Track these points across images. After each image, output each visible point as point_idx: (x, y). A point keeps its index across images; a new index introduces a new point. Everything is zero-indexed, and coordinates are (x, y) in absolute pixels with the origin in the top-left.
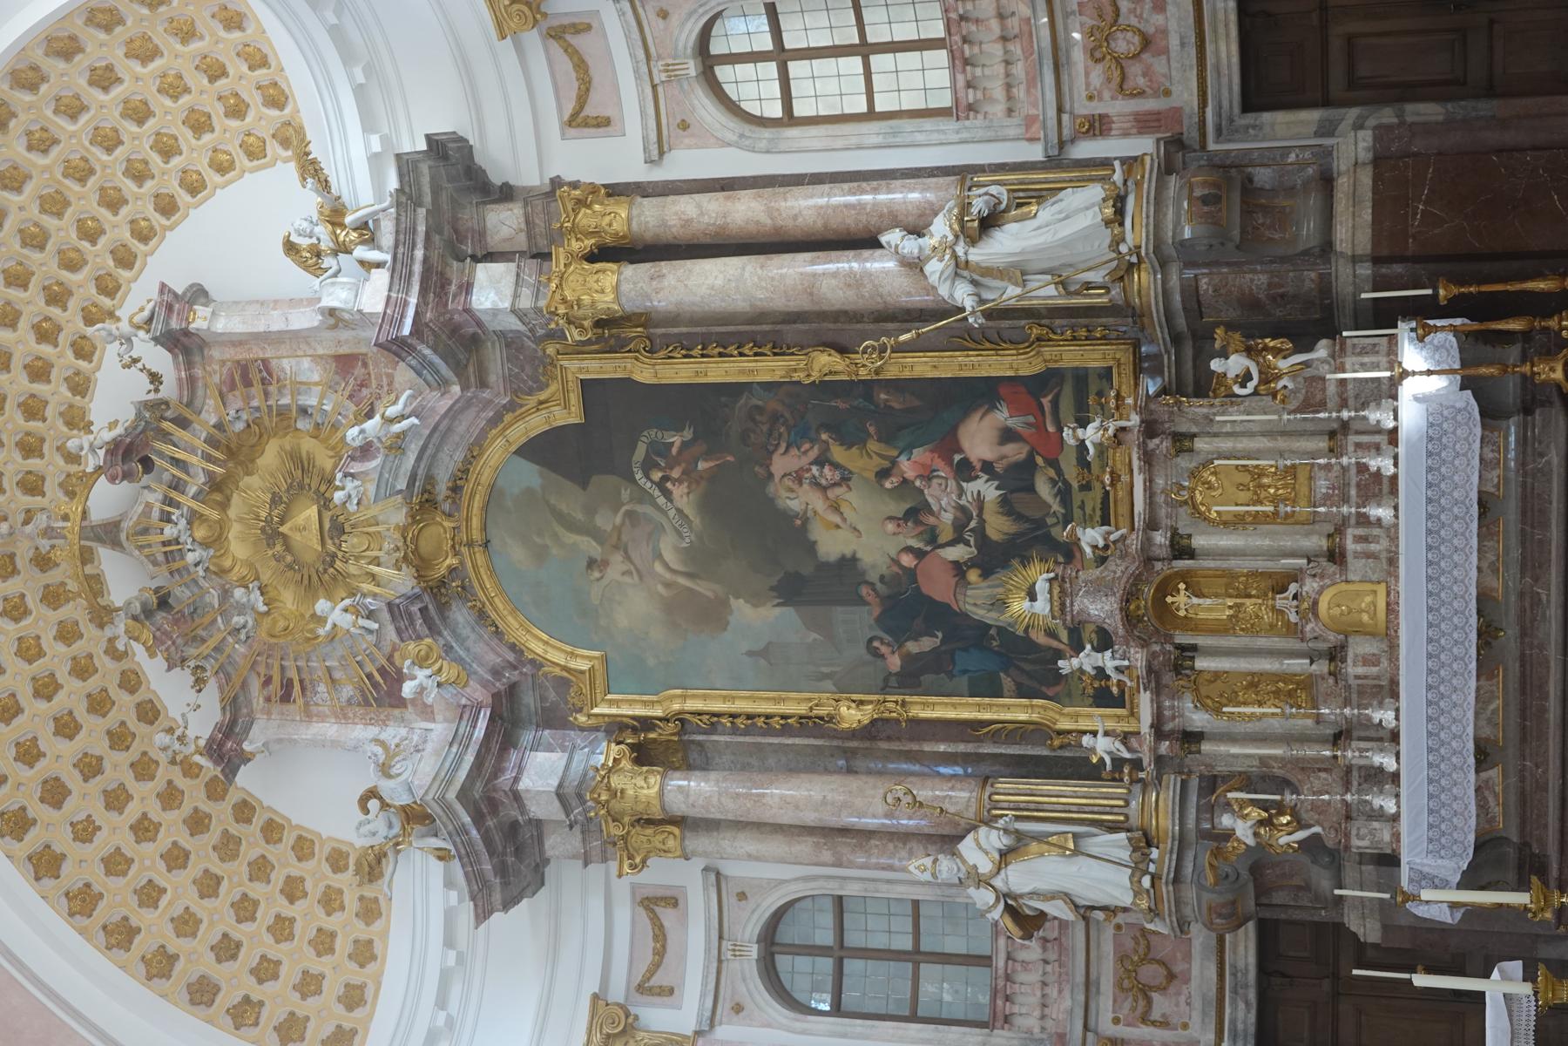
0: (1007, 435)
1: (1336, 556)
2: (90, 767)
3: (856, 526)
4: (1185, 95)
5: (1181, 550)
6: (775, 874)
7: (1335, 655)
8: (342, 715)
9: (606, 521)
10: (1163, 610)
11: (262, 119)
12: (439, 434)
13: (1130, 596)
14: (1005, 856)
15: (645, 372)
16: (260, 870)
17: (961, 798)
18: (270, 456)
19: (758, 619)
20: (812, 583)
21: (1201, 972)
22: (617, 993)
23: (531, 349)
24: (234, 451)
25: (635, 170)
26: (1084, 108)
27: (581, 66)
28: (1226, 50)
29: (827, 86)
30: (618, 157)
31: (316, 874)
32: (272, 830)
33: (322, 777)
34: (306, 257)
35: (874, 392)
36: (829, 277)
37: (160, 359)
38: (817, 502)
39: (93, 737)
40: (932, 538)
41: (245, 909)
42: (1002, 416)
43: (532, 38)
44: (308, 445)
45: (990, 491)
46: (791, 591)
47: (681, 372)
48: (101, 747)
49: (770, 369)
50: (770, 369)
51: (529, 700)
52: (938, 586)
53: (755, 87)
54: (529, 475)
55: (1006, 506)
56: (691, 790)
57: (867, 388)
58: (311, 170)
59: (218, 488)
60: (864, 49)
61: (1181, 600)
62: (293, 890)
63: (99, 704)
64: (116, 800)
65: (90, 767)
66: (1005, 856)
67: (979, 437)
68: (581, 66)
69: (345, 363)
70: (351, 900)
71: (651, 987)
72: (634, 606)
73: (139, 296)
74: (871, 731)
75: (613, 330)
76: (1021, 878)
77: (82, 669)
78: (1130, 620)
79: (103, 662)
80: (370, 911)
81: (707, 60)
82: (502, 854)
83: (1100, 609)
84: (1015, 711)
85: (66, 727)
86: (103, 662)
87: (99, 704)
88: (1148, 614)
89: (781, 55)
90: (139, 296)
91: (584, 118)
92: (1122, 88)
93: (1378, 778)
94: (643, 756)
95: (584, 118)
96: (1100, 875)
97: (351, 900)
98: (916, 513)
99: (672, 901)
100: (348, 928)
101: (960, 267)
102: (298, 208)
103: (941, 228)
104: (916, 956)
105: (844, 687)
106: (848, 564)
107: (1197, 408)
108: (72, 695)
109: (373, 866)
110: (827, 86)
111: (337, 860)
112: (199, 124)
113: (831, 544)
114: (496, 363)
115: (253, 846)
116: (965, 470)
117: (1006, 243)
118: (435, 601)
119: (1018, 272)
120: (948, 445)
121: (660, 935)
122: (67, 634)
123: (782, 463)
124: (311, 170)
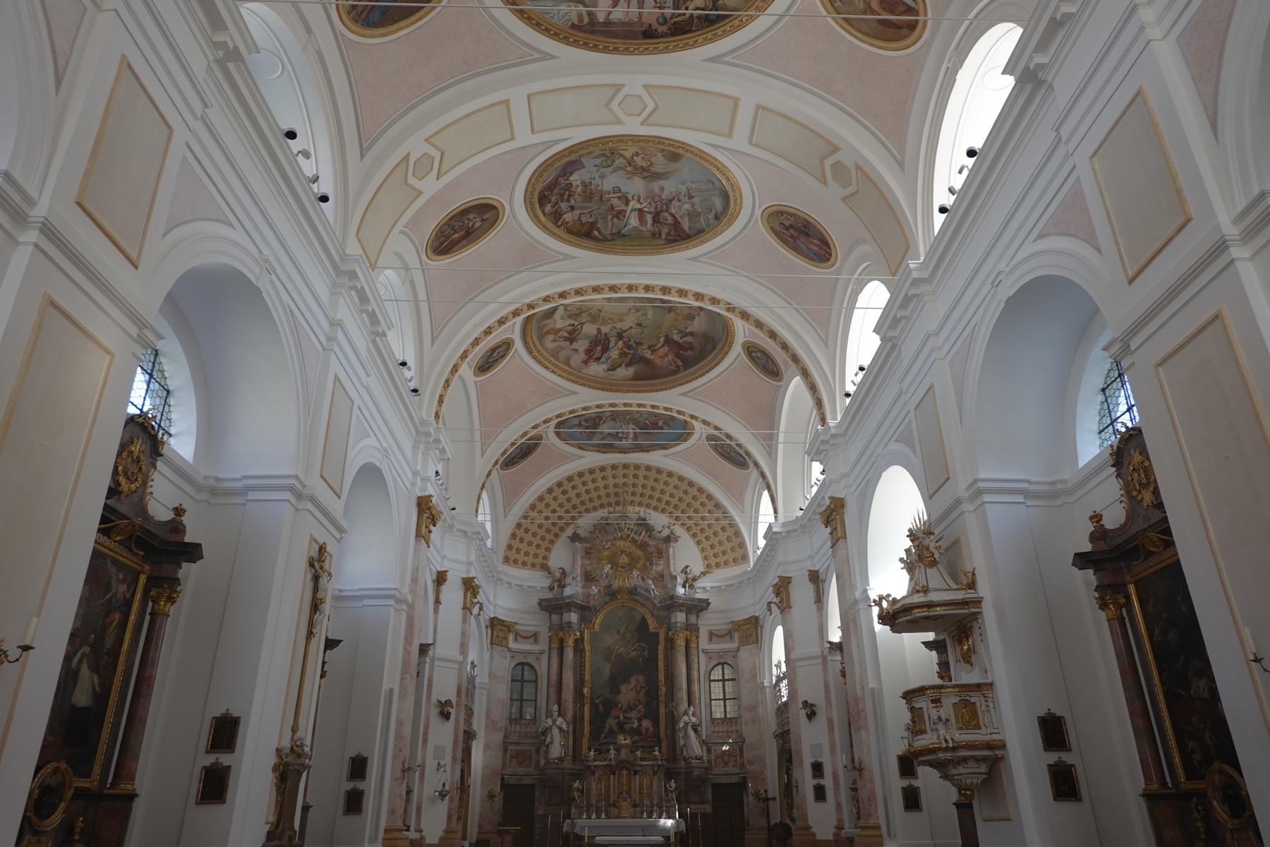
0: (647, 730)
1: (635, 806)
2: (569, 500)
3: (627, 694)
4: (715, 771)
5: (636, 773)
6: (542, 668)
7: (614, 806)
8: (582, 566)
9: (628, 635)
10: (622, 769)
11: (713, 561)
12: (648, 599)
13: (626, 761)
14: (560, 728)
15: (661, 647)
16: (543, 538)
17: (569, 715)
18: (639, 552)
19: (607, 669)
20: (615, 682)
21: (522, 771)
22: (518, 627)
23: (665, 621)
24: (643, 546)
25: (701, 647)
26: (713, 748)
27: (723, 636)
28: (724, 780)
29: (717, 690)
30: (704, 643)
31: (542, 552)
32: (552, 542)
33: (560, 556)
34: (684, 571)
35: (659, 700)
36: (683, 694)
37: (666, 533)
38: (633, 685)
39: (576, 501)
40: (625, 712)
41: (535, 535)
42: (651, 729)
43: (729, 627)
44: (642, 562)
45: (635, 726)
46: (613, 678)
47: (661, 656)
48: (573, 502)
49: (662, 677)
50: (662, 677)
51: (587, 613)
52: (614, 712)
53: (717, 674)
54: (638, 618)
55: (632, 729)
56: (569, 654)
57: (657, 698)
58: (703, 574)
59: (634, 541)
60: (724, 699)
61: (624, 772)
62: (538, 546)
63: (582, 503)
64: (561, 505)
65: (569, 500)
66: (560, 728)
67: (646, 723)
68: (723, 636)
69: (662, 576)
70: (536, 561)
71: (517, 634)
72: (610, 640)
73: (679, 530)
74: (582, 695)
75: (670, 642)
76: (555, 731)
77: (591, 500)
78: (621, 762)
79: (592, 505)
80: (533, 565)
81: (723, 664)
82: (553, 606)
83: (624, 754)
84: (587, 729)
85: (578, 495)
86: (592, 505)
87: (582, 503)
88: (622, 765)
89: (724, 680)
90: (679, 530)
91: (712, 635)
92: (717, 757)
93: (598, 817)
94: (576, 641)
95: (712, 635)
96: (556, 751)
97: (536, 561)
98: (630, 708)
99: (536, 641)
100: (530, 560)
101: (687, 724)
102: (697, 567)
103: (694, 719)
104: (522, 700)
105: (592, 689)
106: (619, 692)
107: (662, 776)
108: (585, 497)
109: (544, 567)
110: (717, 690)
111: (545, 558)
112: (712, 546)
113: (623, 688)
114: (662, 613)
115: (549, 537)
116: (640, 720)
117: (692, 734)
118: (612, 594)
119: (686, 736)
120: (645, 716)
121: (528, 638)
122: (599, 497)
123: (641, 678)
124: (703, 574)
